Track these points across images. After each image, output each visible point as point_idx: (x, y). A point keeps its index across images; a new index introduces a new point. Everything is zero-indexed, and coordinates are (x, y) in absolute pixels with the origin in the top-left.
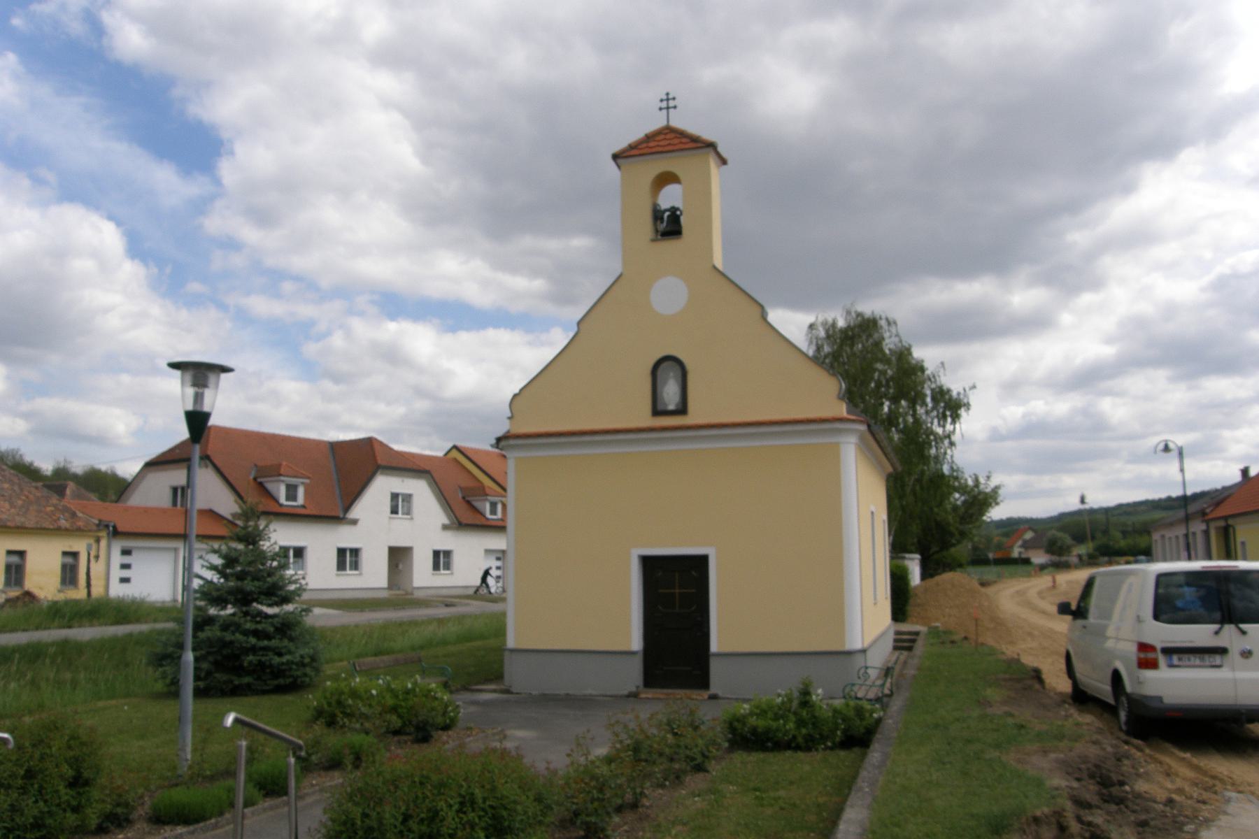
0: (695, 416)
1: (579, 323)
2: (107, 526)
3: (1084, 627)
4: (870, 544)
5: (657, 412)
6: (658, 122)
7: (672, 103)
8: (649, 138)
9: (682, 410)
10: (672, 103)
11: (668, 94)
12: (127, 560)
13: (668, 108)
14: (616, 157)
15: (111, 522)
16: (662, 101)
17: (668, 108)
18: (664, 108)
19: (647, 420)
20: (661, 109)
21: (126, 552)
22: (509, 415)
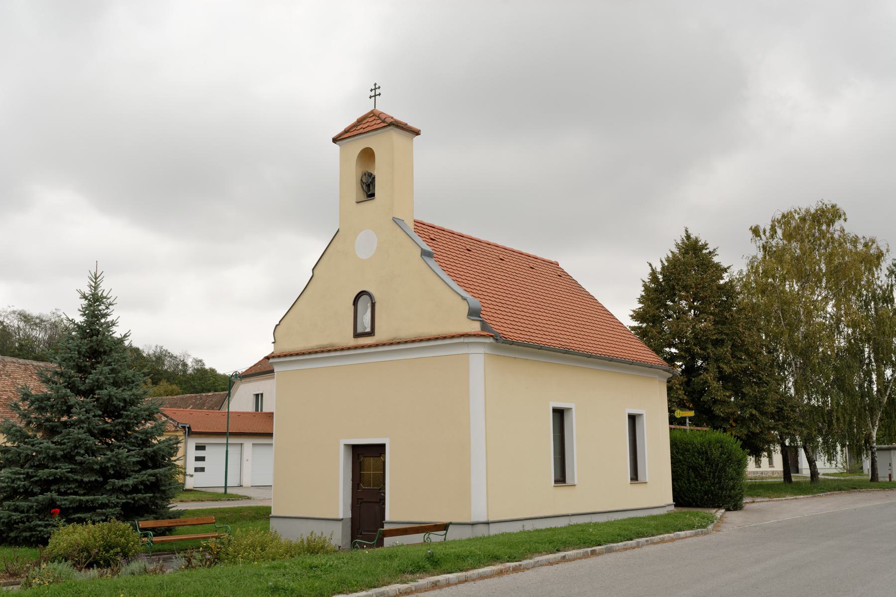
0: (381, 334)
1: (313, 270)
2: (184, 427)
3: (247, 460)
4: (655, 510)
5: (357, 335)
6: (366, 108)
7: (378, 92)
8: (360, 121)
9: (371, 333)
10: (378, 92)
11: (375, 85)
12: (200, 453)
13: (375, 96)
14: (335, 140)
15: (186, 424)
16: (379, 94)
17: (375, 96)
18: (378, 95)
19: (353, 342)
20: (371, 97)
21: (200, 448)
22: (274, 341)
